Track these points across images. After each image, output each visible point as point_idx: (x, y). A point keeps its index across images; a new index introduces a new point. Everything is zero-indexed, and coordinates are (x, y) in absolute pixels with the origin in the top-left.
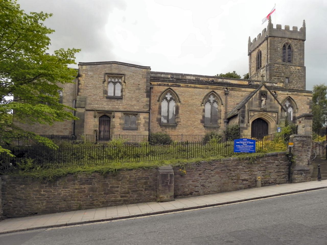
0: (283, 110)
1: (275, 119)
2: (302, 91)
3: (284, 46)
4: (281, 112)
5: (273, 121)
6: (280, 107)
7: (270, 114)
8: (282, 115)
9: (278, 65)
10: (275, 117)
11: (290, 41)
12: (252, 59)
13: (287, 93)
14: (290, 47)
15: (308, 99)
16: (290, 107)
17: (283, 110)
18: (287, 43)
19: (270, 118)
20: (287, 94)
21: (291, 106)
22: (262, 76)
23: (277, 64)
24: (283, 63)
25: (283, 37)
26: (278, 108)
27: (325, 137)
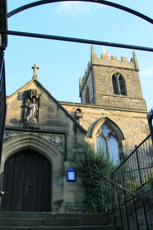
0: (78, 129)
1: (61, 150)
2: (132, 110)
3: (114, 77)
4: (75, 135)
5: (56, 153)
6: (71, 124)
7: (47, 137)
8: (76, 139)
9: (107, 97)
10: (61, 144)
11: (119, 71)
12: (83, 100)
13: (102, 111)
14: (121, 78)
15: (142, 122)
16: (112, 138)
17: (78, 129)
18: (117, 74)
19: (51, 148)
20: (103, 114)
21: (113, 135)
22: (33, 68)
23: (106, 96)
24: (115, 95)
25: (111, 66)
26: (67, 125)
27: (15, 83)
